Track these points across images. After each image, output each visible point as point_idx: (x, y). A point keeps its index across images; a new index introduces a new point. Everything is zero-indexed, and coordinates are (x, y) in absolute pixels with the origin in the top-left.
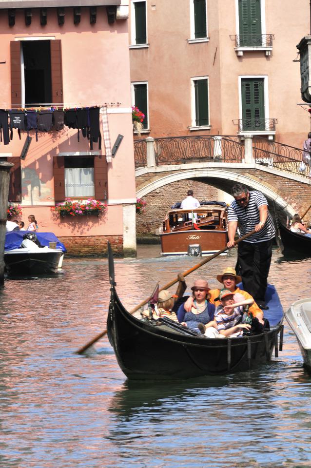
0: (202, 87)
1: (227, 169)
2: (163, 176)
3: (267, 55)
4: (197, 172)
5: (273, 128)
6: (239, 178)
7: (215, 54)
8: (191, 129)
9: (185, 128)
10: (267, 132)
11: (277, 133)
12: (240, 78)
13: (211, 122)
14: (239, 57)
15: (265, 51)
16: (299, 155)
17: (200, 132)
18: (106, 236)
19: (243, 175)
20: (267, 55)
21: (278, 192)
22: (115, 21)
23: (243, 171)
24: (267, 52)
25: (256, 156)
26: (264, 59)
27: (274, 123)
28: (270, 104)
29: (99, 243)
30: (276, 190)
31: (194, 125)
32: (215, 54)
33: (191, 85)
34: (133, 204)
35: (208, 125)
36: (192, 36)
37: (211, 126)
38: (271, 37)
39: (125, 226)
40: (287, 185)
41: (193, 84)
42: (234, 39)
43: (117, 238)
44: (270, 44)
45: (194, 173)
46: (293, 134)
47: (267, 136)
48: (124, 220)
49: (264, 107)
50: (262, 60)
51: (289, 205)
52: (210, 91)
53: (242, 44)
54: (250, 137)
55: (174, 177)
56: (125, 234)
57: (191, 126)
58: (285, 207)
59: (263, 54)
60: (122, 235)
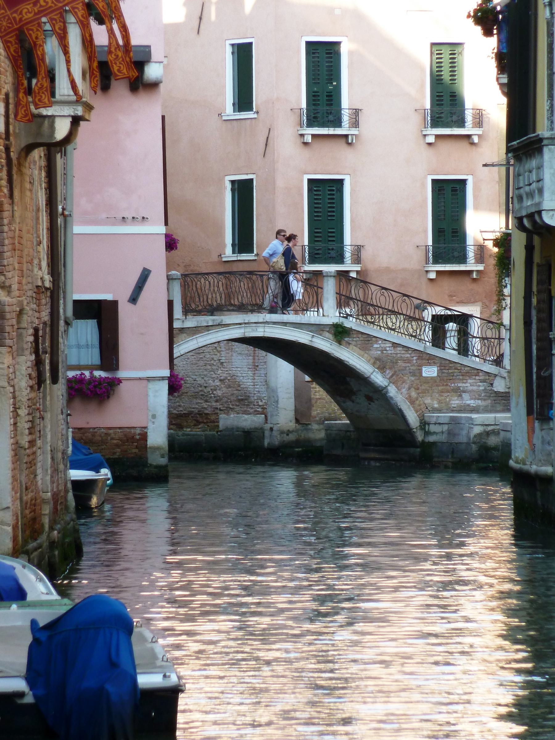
0: (243, 191)
1: (297, 326)
2: (194, 334)
3: (350, 142)
4: (248, 330)
5: (357, 259)
6: (314, 340)
7: (268, 138)
8: (224, 259)
9: (215, 258)
10: (348, 266)
11: (364, 269)
12: (430, 178)
13: (257, 248)
14: (306, 144)
15: (346, 136)
16: (409, 306)
17: (240, 264)
18: (120, 428)
19: (321, 335)
20: (350, 142)
21: (374, 364)
22: (140, 85)
23: (318, 329)
24: (350, 137)
25: (340, 305)
26: (345, 145)
27: (358, 251)
28: (352, 221)
29: (109, 438)
30: (372, 361)
31: (228, 253)
32: (268, 138)
33: (225, 188)
34: (163, 378)
35: (253, 253)
36: (229, 108)
37: (257, 255)
38: (356, 113)
39: (150, 414)
40: (389, 352)
41: (229, 186)
42: (478, 117)
43: (138, 431)
44: (355, 124)
45: (242, 331)
46: (388, 270)
47: (470, 272)
48: (149, 403)
49: (343, 225)
50: (340, 148)
51: (391, 384)
52: (256, 199)
53: (310, 124)
54: (332, 274)
55: (210, 337)
56: (151, 426)
57: (225, 254)
58: (385, 388)
59: (343, 141)
60: (146, 428)
